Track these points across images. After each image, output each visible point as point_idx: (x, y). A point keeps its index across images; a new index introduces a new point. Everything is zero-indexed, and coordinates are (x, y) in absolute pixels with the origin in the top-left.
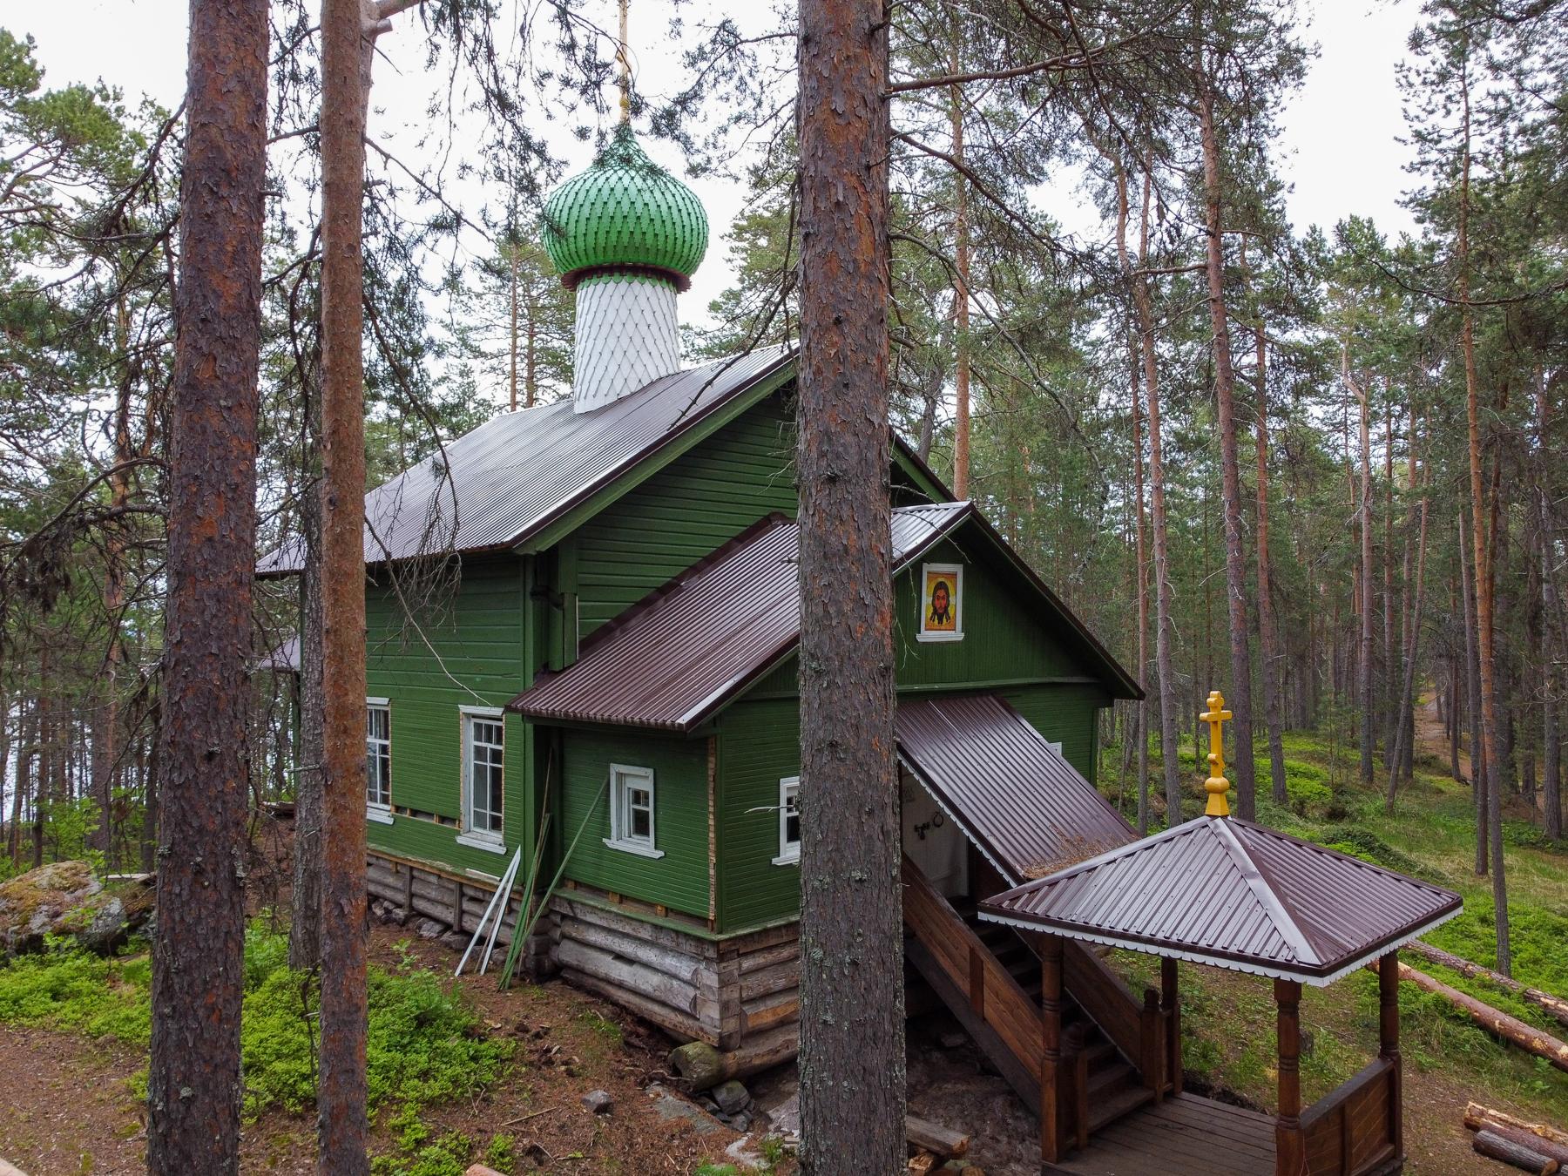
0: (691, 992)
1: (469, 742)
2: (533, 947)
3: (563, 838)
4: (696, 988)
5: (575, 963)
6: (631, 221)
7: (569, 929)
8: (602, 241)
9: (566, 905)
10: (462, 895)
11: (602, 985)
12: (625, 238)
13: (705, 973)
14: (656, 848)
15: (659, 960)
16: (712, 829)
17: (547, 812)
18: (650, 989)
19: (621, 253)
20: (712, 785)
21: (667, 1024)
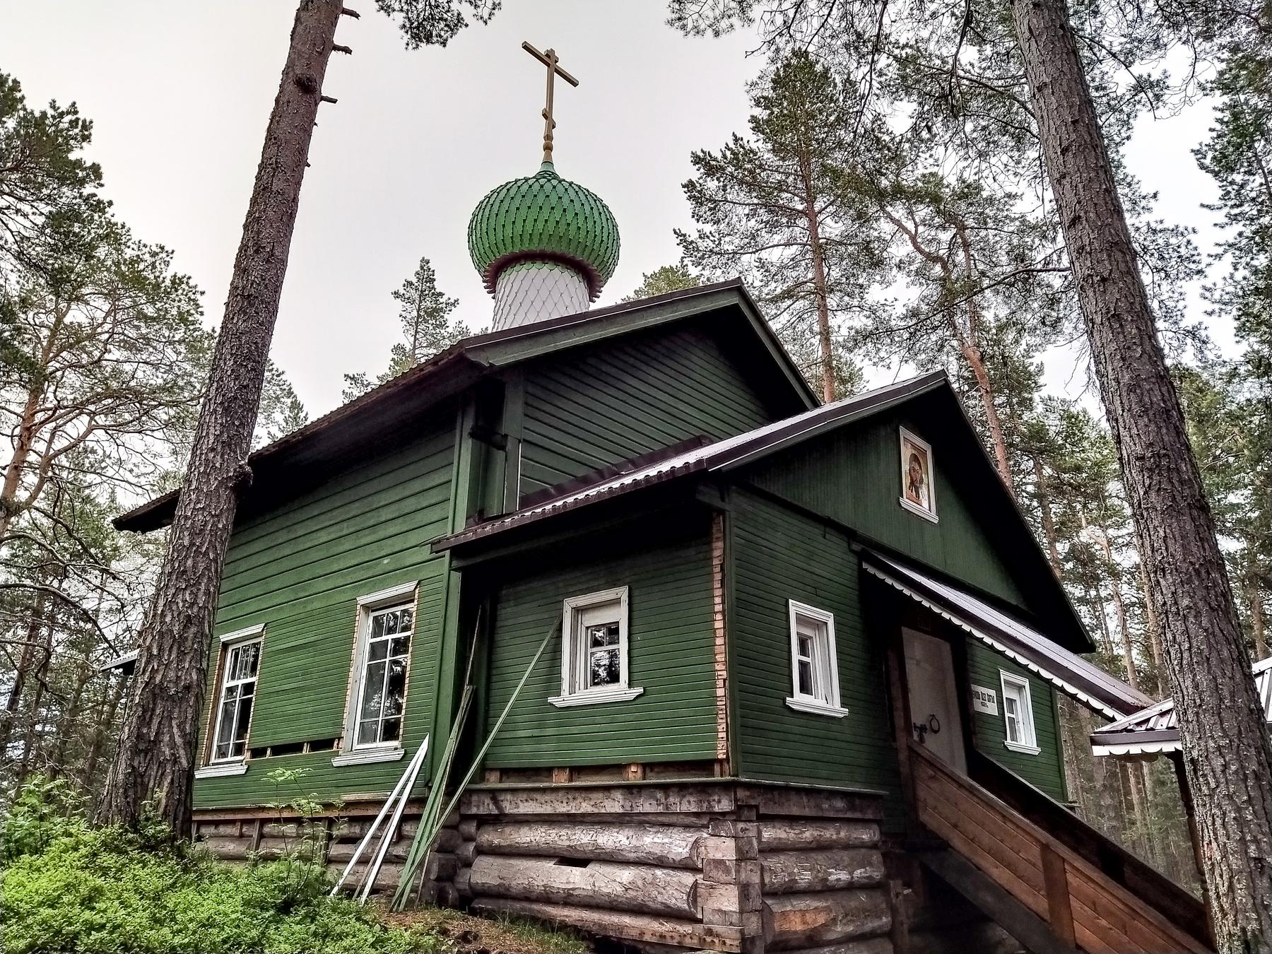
2: (435, 868)
3: (487, 718)
4: (695, 870)
5: (495, 882)
7: (491, 837)
8: (529, 228)
9: (488, 801)
13: (712, 842)
15: (634, 842)
16: (720, 633)
17: (470, 683)
20: (718, 577)
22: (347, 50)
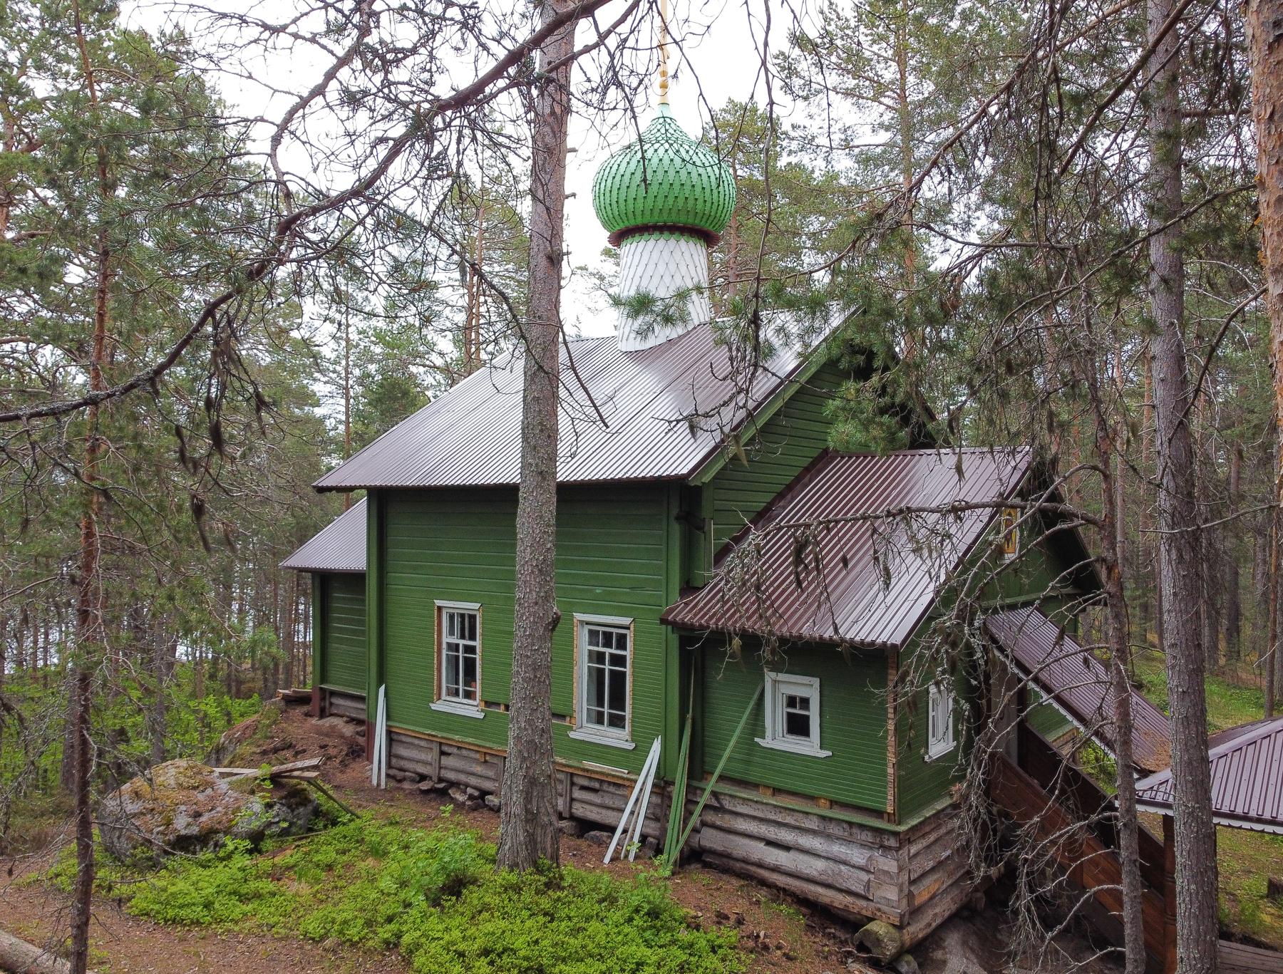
0: (865, 877)
1: (583, 646)
4: (868, 872)
6: (688, 188)
8: (631, 206)
10: (573, 784)
11: (753, 869)
12: (681, 202)
13: (881, 859)
14: (821, 748)
18: (815, 873)
19: (674, 215)
21: (836, 904)
22: (574, 195)
